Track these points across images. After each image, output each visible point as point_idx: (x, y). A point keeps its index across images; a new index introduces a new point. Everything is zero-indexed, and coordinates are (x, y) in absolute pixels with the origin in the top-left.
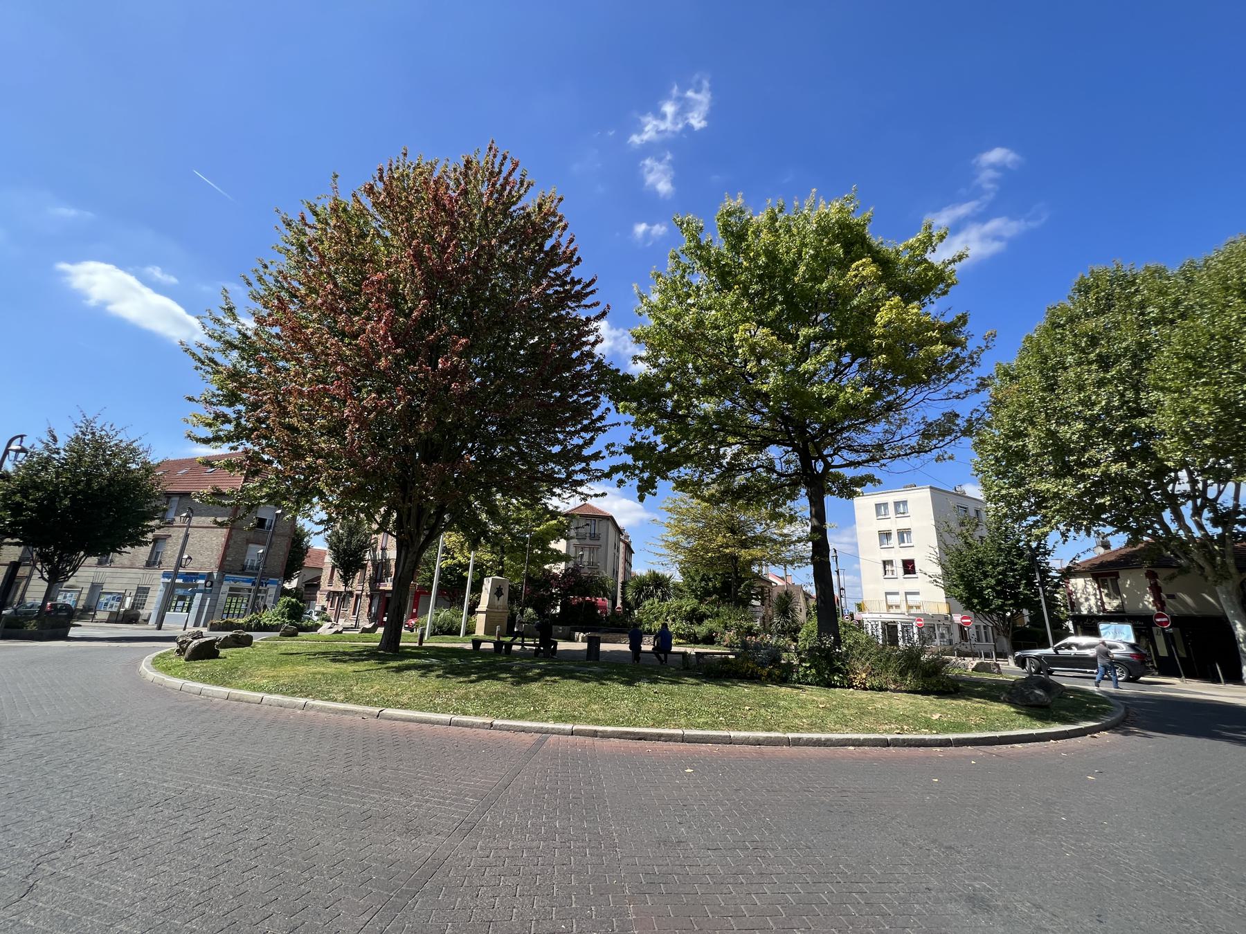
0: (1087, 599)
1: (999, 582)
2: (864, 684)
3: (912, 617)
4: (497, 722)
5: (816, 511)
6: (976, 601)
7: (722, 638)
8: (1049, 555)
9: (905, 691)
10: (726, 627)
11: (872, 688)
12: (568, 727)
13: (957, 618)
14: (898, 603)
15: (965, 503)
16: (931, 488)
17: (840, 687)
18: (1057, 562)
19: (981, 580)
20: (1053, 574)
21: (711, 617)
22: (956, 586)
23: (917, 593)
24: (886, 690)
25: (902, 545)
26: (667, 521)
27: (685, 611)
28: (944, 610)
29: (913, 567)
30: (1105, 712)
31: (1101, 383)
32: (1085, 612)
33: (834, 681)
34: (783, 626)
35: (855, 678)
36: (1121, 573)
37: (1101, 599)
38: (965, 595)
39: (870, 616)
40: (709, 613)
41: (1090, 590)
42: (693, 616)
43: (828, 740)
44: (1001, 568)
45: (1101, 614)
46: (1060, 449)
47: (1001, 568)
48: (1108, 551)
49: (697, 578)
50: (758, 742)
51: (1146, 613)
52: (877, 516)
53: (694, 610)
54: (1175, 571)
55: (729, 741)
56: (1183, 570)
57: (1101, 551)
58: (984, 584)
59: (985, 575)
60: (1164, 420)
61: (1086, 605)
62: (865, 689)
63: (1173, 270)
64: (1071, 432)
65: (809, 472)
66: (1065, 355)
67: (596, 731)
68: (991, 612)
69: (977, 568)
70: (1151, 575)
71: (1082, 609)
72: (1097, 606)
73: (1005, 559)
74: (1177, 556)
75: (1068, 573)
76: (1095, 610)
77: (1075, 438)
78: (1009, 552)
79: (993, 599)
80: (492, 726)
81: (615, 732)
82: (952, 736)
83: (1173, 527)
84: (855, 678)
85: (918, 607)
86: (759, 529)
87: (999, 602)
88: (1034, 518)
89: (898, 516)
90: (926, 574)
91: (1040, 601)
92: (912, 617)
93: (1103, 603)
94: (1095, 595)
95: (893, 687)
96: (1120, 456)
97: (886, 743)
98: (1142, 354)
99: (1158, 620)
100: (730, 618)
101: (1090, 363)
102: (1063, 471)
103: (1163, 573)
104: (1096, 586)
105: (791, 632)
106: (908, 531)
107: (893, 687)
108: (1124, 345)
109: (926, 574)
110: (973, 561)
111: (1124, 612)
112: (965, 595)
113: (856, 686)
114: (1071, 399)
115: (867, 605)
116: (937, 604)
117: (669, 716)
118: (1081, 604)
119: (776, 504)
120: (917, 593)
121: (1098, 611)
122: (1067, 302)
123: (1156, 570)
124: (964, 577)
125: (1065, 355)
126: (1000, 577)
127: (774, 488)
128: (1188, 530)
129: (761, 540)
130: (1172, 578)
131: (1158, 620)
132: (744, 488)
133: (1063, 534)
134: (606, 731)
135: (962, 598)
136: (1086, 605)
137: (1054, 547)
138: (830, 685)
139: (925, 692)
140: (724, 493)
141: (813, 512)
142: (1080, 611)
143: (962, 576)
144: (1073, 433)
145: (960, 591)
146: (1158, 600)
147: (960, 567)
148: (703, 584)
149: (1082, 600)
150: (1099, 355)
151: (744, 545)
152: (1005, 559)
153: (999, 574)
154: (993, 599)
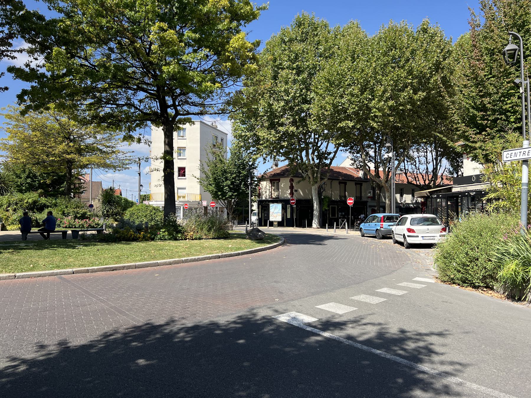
0: (266, 192)
1: (232, 183)
2: (192, 237)
3: (180, 203)
4: (18, 274)
5: (168, 141)
6: (220, 193)
7: (61, 222)
8: (255, 169)
9: (211, 239)
10: (63, 214)
11: (196, 239)
12: (70, 270)
13: (205, 204)
14: (184, 195)
15: (218, 134)
16: (201, 122)
17: (181, 240)
18: (258, 173)
19: (223, 182)
20: (255, 179)
21: (51, 207)
22: (210, 185)
23: (184, 188)
24: (202, 239)
25: (179, 157)
26: (6, 126)
27: (27, 203)
28: (198, 199)
29: (184, 172)
30: (279, 239)
31: (295, 81)
32: (264, 199)
33: (178, 237)
34: (107, 211)
35: (188, 235)
36: (282, 179)
37: (271, 192)
38: (215, 190)
39: (156, 203)
40: (48, 204)
41: (268, 187)
42: (34, 206)
43: (198, 258)
44: (235, 175)
45: (270, 199)
46: (272, 115)
47: (235, 175)
48: (277, 168)
49: (23, 176)
50: (170, 264)
51: (287, 198)
52: (178, 137)
53: (35, 202)
54: (301, 179)
55: (158, 265)
56: (304, 179)
57: (274, 167)
58: (225, 184)
59: (227, 179)
60: (314, 110)
61: (265, 195)
62: (193, 239)
63: (332, 28)
64: (278, 106)
65: (166, 116)
66: (284, 61)
67: (88, 270)
68: (226, 199)
69: (223, 174)
70: (292, 180)
71: (263, 197)
72: (269, 195)
73: (237, 170)
74: (303, 172)
75: (262, 179)
76: (268, 197)
77: (279, 109)
78: (239, 167)
79: (227, 193)
80: (15, 277)
81: (99, 268)
82: (240, 252)
83: (305, 159)
84: (188, 235)
85: (184, 197)
86: (90, 141)
87: (230, 194)
88: (253, 149)
89: (179, 138)
90: (195, 177)
91: (248, 193)
92: (180, 203)
93: (271, 194)
94: (269, 190)
95: (205, 237)
96: (294, 123)
97: (219, 257)
98: (313, 71)
99: (291, 202)
100: (67, 207)
101: (293, 69)
102: (272, 126)
103: (296, 180)
104: (270, 186)
105: (113, 215)
106: (184, 149)
107: (205, 237)
108: (308, 64)
109: (195, 177)
110: (222, 171)
111: (278, 198)
112: (215, 190)
113: (189, 239)
114: (281, 87)
115: (154, 197)
116: (195, 195)
117: (119, 259)
118: (263, 194)
119: (130, 129)
120: (184, 188)
121: (269, 198)
122: (291, 31)
123: (294, 179)
124: (216, 180)
125: (284, 61)
126: (234, 180)
127: (128, 118)
128: (308, 159)
129: (91, 149)
130: (299, 182)
131: (291, 202)
132: (109, 116)
133: (264, 159)
134: (94, 269)
135: (213, 192)
136: (265, 195)
137: (258, 165)
138: (176, 239)
139: (219, 238)
140: (95, 117)
141: (167, 142)
142: (262, 198)
143: (215, 179)
144: (279, 107)
145: (212, 188)
146: (292, 194)
147: (215, 174)
148: (29, 180)
149: (264, 193)
150: (297, 66)
151: (79, 151)
152: (237, 170)
153: (233, 178)
154: (227, 193)
